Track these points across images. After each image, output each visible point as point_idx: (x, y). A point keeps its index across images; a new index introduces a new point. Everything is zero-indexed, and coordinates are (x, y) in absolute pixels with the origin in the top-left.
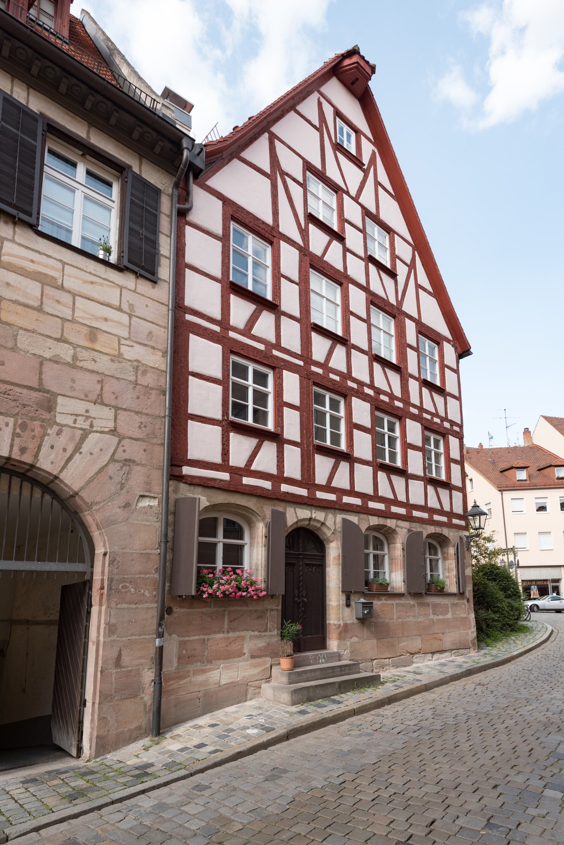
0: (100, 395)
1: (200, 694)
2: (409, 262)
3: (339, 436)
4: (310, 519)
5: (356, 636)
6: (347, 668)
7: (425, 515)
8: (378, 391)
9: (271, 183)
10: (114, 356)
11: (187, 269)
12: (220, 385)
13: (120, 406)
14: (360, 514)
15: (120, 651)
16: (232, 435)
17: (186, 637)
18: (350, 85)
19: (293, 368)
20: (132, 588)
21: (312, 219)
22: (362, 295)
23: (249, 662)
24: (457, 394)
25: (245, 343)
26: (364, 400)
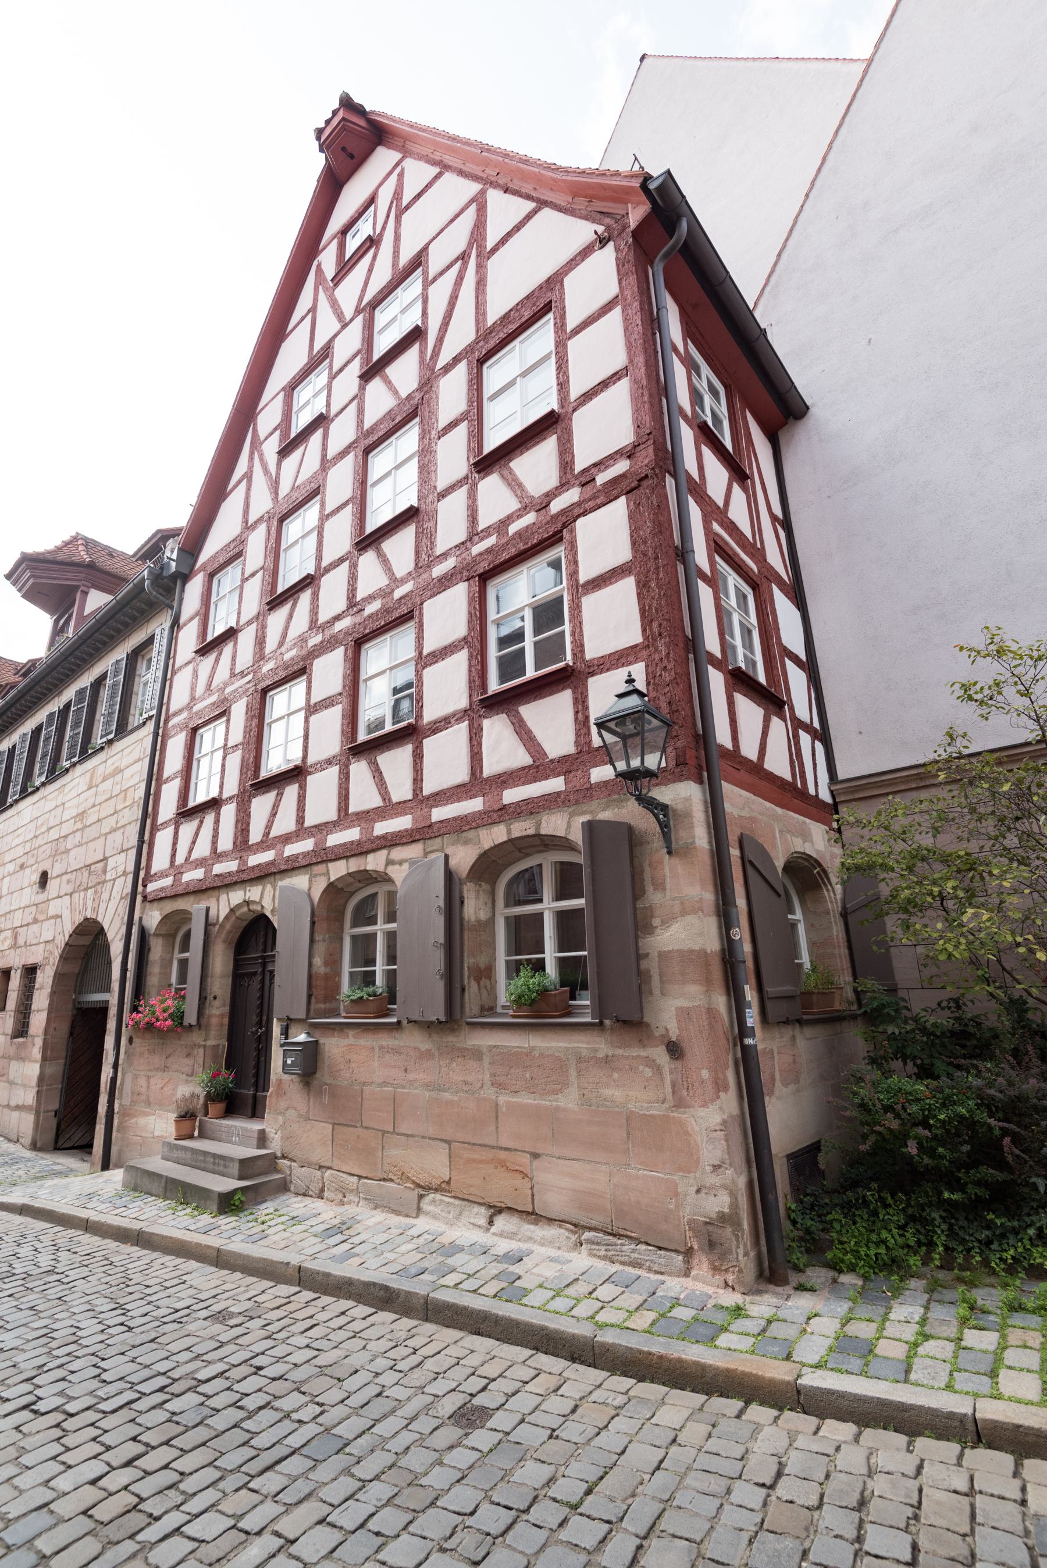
6: (222, 1163)
18: (355, 160)
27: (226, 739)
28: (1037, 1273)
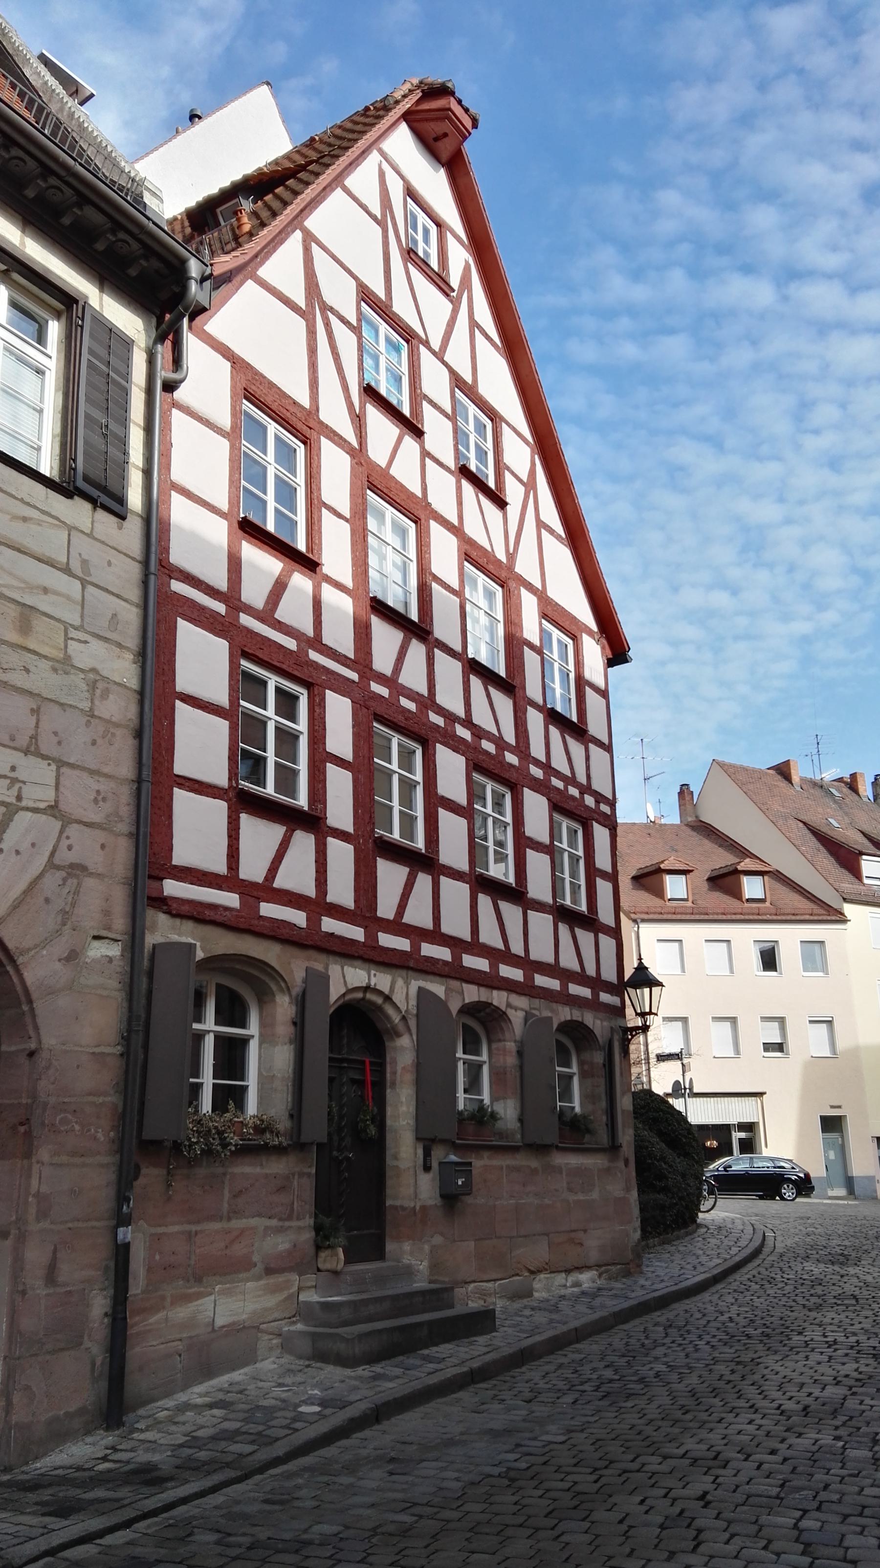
0: (34, 738)
1: (180, 1346)
2: (525, 478)
3: (413, 819)
4: (367, 989)
5: (442, 1234)
7: (554, 984)
8: (479, 733)
9: (307, 325)
10: (57, 661)
11: (173, 493)
12: (225, 719)
13: (65, 759)
14: (448, 980)
15: (55, 1251)
16: (243, 817)
17: (160, 1226)
19: (342, 686)
20: (76, 1123)
21: (370, 392)
22: (452, 541)
23: (262, 1282)
24: (606, 740)
25: (266, 637)
26: (456, 750)
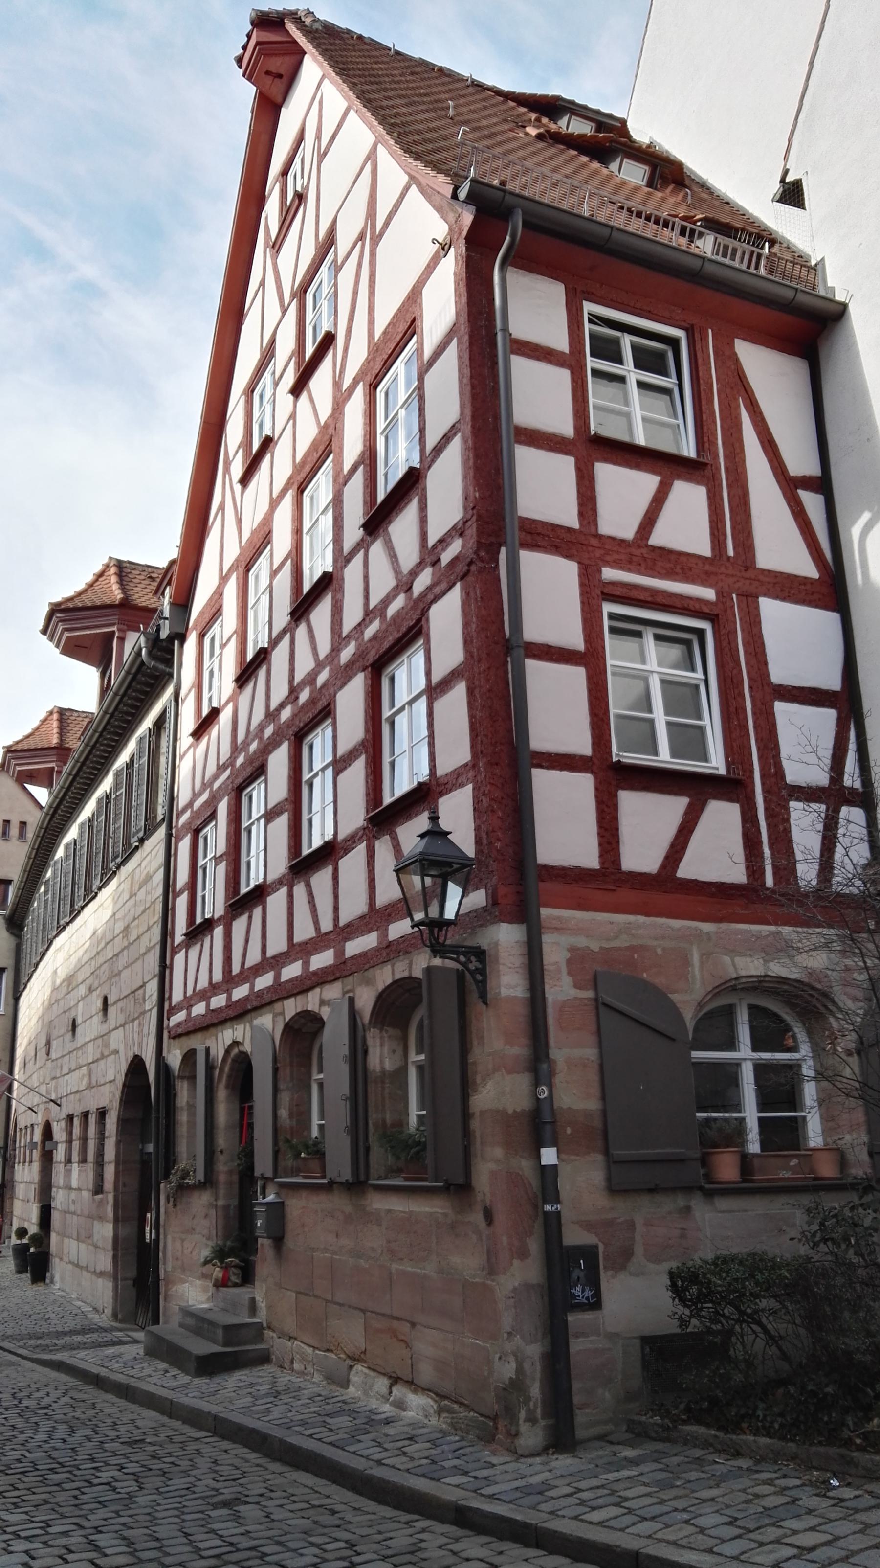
27: (428, 673)
28: (871, 1476)
